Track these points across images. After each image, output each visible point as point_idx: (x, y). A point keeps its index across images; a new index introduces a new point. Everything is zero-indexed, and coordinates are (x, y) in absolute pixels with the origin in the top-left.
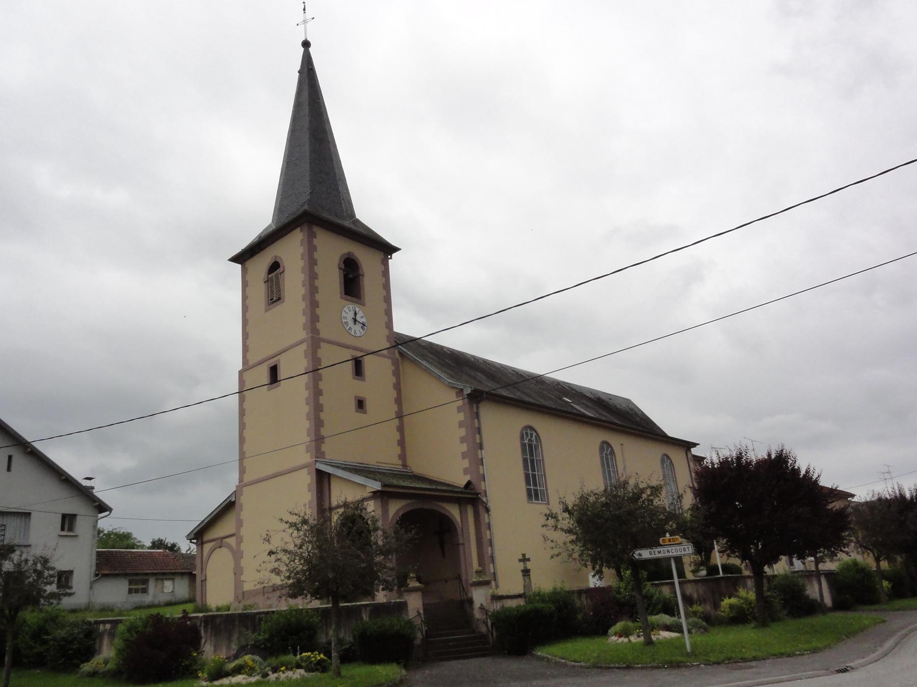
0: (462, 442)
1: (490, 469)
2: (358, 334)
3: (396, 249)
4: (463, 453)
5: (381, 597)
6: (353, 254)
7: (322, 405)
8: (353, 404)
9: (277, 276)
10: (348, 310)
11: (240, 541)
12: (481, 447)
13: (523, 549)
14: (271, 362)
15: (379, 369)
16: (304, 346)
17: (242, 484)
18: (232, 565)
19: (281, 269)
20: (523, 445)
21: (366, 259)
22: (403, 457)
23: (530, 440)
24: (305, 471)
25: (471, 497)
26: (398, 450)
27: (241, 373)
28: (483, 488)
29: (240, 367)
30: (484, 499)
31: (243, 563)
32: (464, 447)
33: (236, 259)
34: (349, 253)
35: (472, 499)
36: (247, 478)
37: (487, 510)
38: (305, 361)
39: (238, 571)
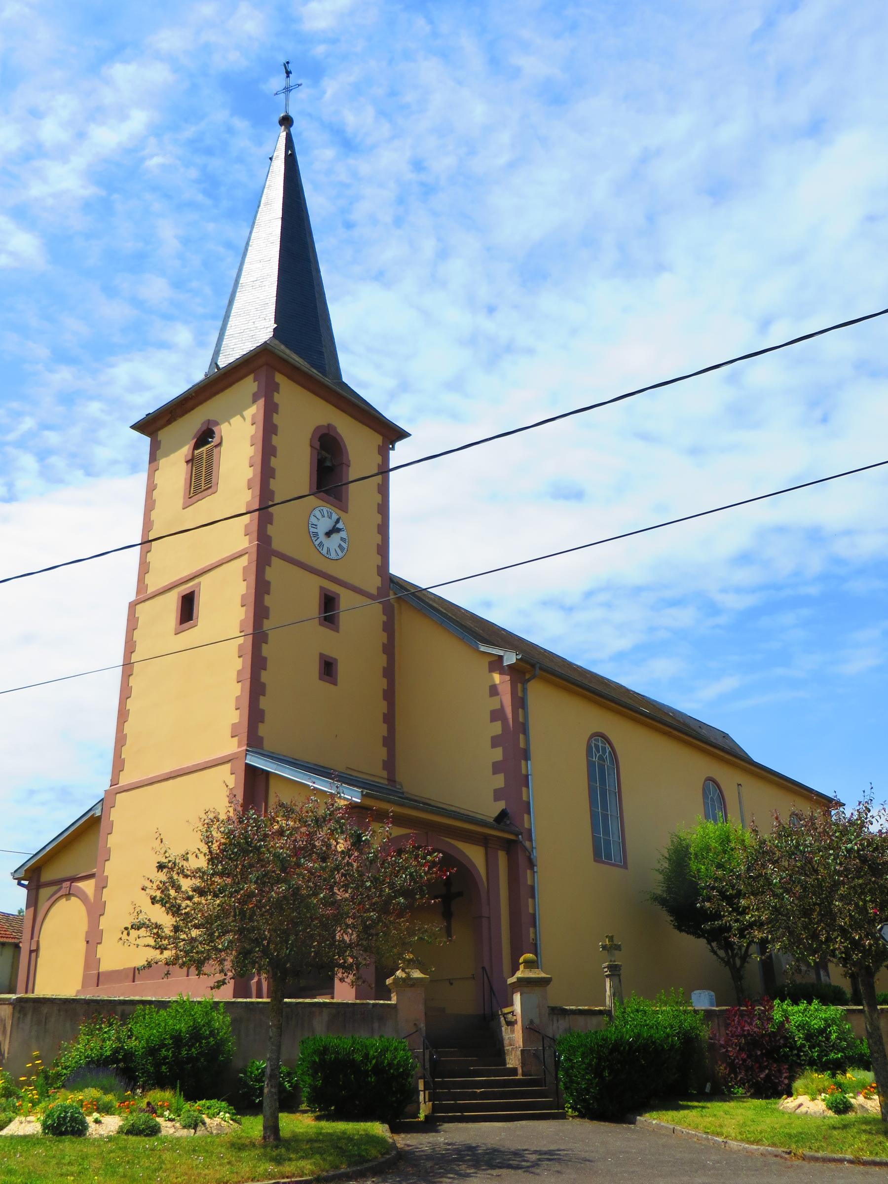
0: (494, 746)
1: (538, 794)
2: (333, 555)
3: (402, 434)
4: (495, 764)
5: (344, 992)
6: (335, 428)
7: (265, 659)
8: (315, 668)
9: (210, 455)
10: (322, 517)
11: (102, 886)
12: (526, 755)
13: (576, 948)
14: (185, 589)
15: (360, 617)
16: (244, 561)
17: (116, 788)
18: (83, 926)
19: (216, 441)
20: (590, 765)
21: (357, 441)
22: (390, 764)
23: (601, 758)
24: (227, 767)
25: (508, 836)
26: (383, 753)
27: (133, 606)
28: (526, 826)
29: (132, 597)
30: (527, 844)
31: (104, 923)
32: (498, 754)
33: (142, 427)
34: (329, 425)
35: (509, 842)
36: (125, 779)
37: (531, 864)
38: (244, 584)
39: (93, 939)
